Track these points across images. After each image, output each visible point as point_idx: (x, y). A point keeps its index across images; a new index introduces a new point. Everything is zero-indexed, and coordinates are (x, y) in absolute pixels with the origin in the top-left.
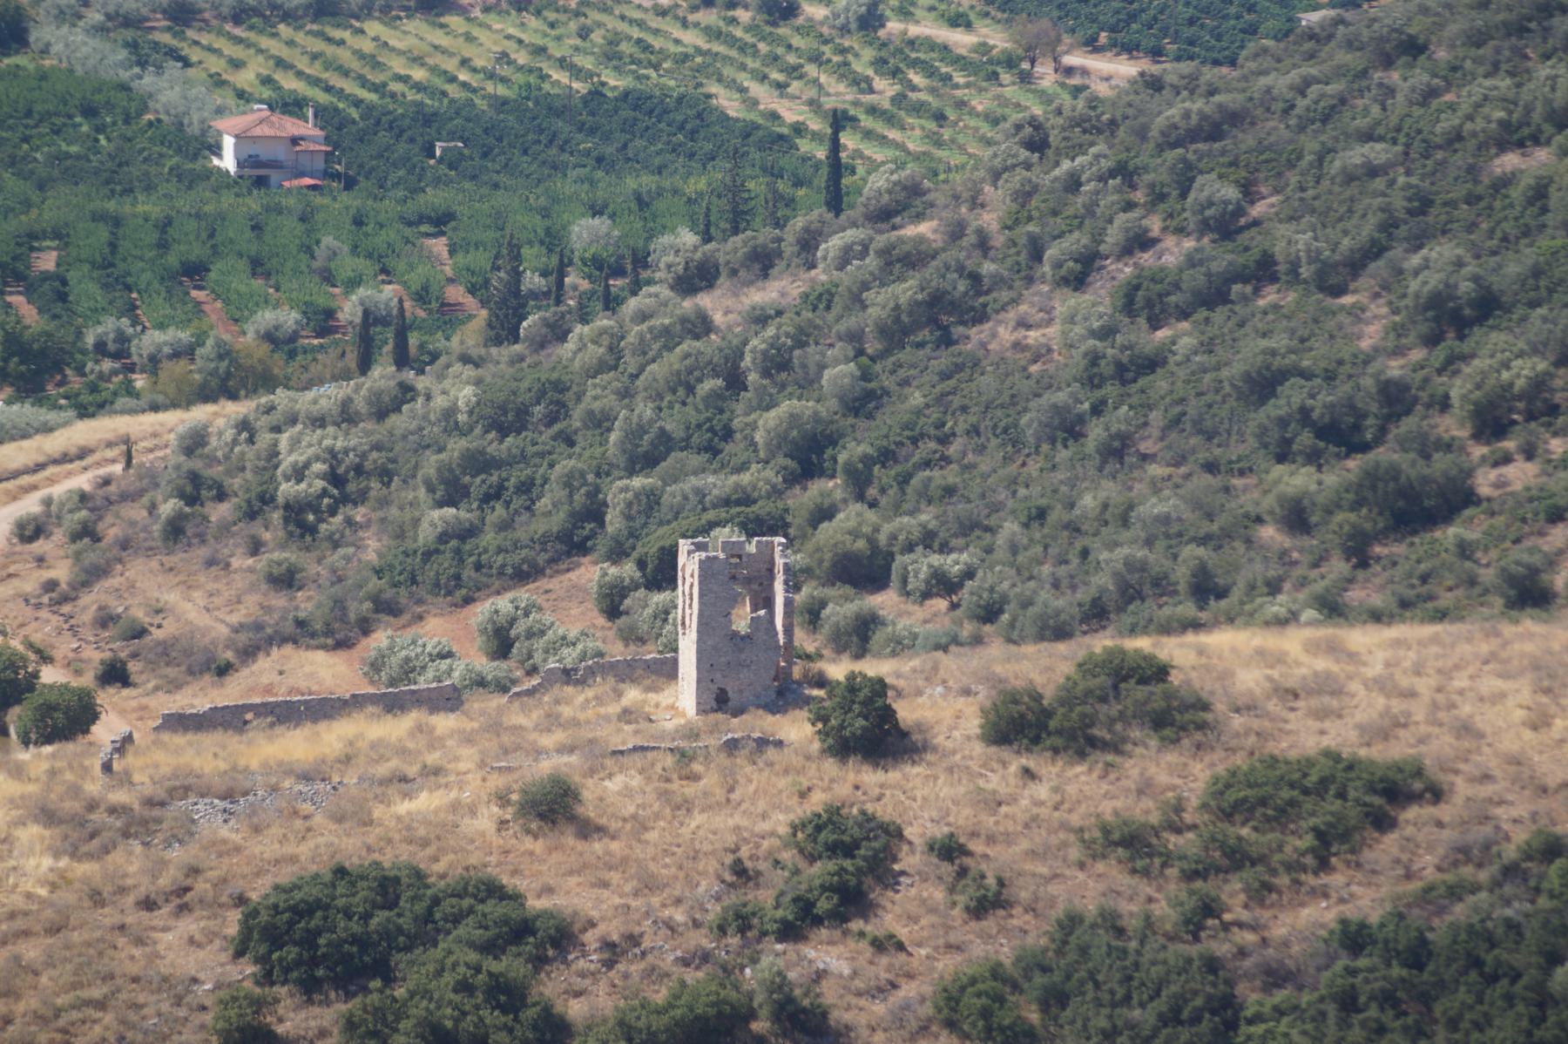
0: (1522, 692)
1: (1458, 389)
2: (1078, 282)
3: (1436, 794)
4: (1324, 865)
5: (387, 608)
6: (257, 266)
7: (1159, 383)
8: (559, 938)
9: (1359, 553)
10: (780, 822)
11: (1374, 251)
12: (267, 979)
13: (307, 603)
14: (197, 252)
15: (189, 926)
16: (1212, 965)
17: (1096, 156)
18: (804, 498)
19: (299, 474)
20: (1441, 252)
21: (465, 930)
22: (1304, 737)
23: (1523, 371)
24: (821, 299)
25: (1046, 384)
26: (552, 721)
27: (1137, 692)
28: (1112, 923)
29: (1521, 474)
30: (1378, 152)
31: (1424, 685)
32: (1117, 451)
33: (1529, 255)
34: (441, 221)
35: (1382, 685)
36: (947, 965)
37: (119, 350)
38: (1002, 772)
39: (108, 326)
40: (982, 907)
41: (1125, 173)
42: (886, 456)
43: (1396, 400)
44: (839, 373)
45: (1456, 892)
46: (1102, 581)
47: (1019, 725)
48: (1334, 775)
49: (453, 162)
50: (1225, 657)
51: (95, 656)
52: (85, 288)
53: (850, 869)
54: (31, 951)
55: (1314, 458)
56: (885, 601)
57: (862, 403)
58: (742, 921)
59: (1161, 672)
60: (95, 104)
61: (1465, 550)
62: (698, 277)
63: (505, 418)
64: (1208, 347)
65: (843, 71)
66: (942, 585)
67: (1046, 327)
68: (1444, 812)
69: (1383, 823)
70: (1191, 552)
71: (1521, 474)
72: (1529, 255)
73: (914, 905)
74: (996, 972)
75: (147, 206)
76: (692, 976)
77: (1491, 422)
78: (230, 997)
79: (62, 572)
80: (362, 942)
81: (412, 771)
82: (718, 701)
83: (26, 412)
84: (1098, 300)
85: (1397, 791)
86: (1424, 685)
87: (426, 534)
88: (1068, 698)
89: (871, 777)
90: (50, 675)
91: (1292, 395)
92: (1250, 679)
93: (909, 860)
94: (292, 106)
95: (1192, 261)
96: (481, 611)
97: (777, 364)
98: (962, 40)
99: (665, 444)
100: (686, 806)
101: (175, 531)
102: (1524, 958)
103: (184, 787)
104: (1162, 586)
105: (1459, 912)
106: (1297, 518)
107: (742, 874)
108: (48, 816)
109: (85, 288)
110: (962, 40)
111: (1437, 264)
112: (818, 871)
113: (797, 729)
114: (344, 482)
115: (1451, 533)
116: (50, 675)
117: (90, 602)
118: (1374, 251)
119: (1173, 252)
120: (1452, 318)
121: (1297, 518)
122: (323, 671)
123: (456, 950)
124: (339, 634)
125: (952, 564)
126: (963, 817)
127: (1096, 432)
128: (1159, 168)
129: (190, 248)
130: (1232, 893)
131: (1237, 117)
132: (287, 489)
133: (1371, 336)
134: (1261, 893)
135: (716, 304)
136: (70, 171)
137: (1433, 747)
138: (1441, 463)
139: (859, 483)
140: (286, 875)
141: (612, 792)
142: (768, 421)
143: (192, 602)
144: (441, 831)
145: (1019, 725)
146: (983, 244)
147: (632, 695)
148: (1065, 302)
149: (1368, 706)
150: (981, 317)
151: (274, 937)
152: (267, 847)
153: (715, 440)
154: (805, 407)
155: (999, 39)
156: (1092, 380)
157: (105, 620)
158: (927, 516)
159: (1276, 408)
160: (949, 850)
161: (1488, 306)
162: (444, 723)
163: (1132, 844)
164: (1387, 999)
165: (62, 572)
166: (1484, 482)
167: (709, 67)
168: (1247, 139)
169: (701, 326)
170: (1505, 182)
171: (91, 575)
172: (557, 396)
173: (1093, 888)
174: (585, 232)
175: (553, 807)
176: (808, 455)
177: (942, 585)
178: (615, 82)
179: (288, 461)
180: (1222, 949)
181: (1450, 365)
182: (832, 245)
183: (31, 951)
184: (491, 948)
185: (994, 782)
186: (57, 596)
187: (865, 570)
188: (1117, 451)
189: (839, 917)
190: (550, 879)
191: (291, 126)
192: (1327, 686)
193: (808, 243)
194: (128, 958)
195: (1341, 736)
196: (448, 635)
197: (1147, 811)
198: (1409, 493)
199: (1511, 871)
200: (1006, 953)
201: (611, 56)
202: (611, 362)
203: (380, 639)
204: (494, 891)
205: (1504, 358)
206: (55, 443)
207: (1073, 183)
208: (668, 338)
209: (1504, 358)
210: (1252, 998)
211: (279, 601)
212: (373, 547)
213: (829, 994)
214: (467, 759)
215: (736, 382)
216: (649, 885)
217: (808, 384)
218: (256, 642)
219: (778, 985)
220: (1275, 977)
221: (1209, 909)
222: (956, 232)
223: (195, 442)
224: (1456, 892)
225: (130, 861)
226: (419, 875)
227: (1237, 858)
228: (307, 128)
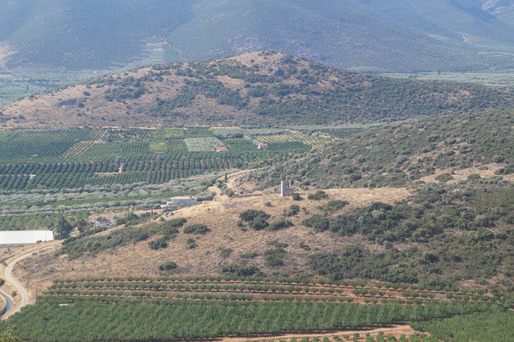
0: (357, 195)
1: (361, 168)
2: (329, 158)
3: (348, 204)
4: (338, 210)
5: (266, 187)
6: (261, 157)
7: (335, 167)
8: (269, 216)
9: (351, 182)
10: (289, 206)
11: (355, 155)
12: (242, 220)
13: (259, 187)
14: (255, 155)
15: (236, 215)
16: (327, 219)
17: (331, 147)
18: (303, 177)
19: (259, 175)
20: (360, 156)
21: (260, 215)
22: (337, 199)
23: (366, 166)
24: (306, 160)
25: (325, 167)
26: (270, 197)
27: (321, 194)
28: (318, 215)
29: (366, 175)
30: (356, 147)
31: (348, 194)
32: (331, 173)
33: (368, 156)
34: (278, 153)
35: (344, 194)
36: (303, 219)
37: (247, 164)
38: (309, 202)
39: (246, 162)
40: (306, 214)
41: (333, 149)
42: (310, 174)
43: (356, 168)
44: (307, 166)
45: (349, 213)
46: (328, 185)
47: (311, 197)
48: (339, 202)
49: (279, 148)
50: (331, 191)
51: (240, 191)
52: (245, 159)
53: (295, 210)
54: (221, 217)
55: (348, 174)
56: (309, 187)
57: (309, 169)
58: (285, 215)
59: (324, 193)
60: (248, 143)
61: (360, 182)
62: (296, 158)
63: (278, 170)
64: (339, 164)
65: (315, 140)
66: (315, 185)
67: (326, 162)
68: (349, 205)
69: (343, 206)
70: (336, 182)
71: (366, 175)
72: (368, 156)
73: (301, 214)
74: (307, 220)
75: (251, 152)
76: (280, 220)
77: (364, 171)
78: (239, 221)
79: (238, 184)
80: (251, 217)
81: (340, 205)
82: (284, 195)
83: (238, 170)
84: (330, 160)
85: (344, 204)
86: (348, 194)
87: (270, 181)
88: (315, 195)
89: (297, 202)
90: (236, 193)
91: (346, 168)
92: (332, 193)
93: (301, 209)
94: (265, 143)
95: (338, 156)
96: (274, 188)
97: (302, 165)
98: (326, 137)
99: (291, 172)
100: (280, 205)
101: (248, 180)
102: (355, 218)
103: (236, 203)
104: (334, 185)
105: (349, 214)
106: (346, 179)
107: (285, 211)
108: (224, 205)
109: (245, 159)
110: (326, 137)
111: (360, 157)
112: (292, 210)
113: (291, 198)
114: (263, 176)
115: (359, 181)
116: (236, 193)
117: (240, 186)
118: (355, 155)
119: (337, 156)
120: (361, 161)
121: (346, 179)
122: (260, 192)
123: (259, 218)
124: (262, 190)
125: (315, 183)
126: (305, 206)
127: (329, 171)
128: (336, 148)
129: (255, 155)
130: (329, 213)
131: (343, 144)
132: (258, 176)
133: (354, 163)
134: (332, 213)
135: (297, 160)
136: (245, 148)
137: (348, 199)
138: (359, 174)
139: (308, 176)
140: (244, 211)
141: (274, 203)
142: (300, 171)
143: (249, 186)
144: (259, 207)
145: (311, 197)
146: (321, 155)
147: (277, 194)
148: (327, 160)
149: (343, 196)
150: (320, 161)
151: (243, 216)
152: (243, 208)
153: (295, 172)
154: (304, 169)
155: (329, 137)
156: (329, 167)
157: (241, 188)
158: (313, 179)
159: (345, 169)
160: (304, 209)
161: (364, 160)
162: (260, 197)
163: (321, 208)
164: (342, 222)
165: (238, 184)
166: (363, 176)
167: (303, 139)
168: (344, 145)
169: (296, 162)
170: (366, 149)
171: (240, 184)
172: (282, 168)
173: (317, 212)
174: (290, 154)
175: (269, 205)
176: (304, 173)
177: (315, 185)
178: (295, 141)
179: (259, 174)
180: (328, 218)
181: (361, 166)
182: (307, 155)
183: (221, 217)
184: (262, 217)
185: (308, 203)
186: (238, 186)
187: (308, 184)
188: (331, 173)
189: (293, 214)
190: (268, 211)
191: (265, 145)
192: (339, 194)
193: (305, 155)
194: (230, 218)
195: (340, 199)
196: (271, 189)
197: (322, 205)
198: (356, 177)
199: (354, 211)
200: (308, 218)
201: (295, 138)
202: (287, 165)
203: (265, 190)
204: (263, 212)
205: (365, 165)
206: (240, 172)
207: (329, 149)
208: (292, 163)
209: (365, 165)
210: (330, 222)
211: (257, 186)
212: (265, 181)
213: (292, 222)
214: (261, 200)
215: (298, 167)
216: (277, 212)
217: (304, 167)
218: (254, 190)
219: (288, 221)
220: (333, 220)
221: (327, 214)
222: (318, 154)
223: (251, 172)
224: (349, 213)
225: (231, 209)
226: (256, 211)
227: (330, 209)
228: (266, 145)
